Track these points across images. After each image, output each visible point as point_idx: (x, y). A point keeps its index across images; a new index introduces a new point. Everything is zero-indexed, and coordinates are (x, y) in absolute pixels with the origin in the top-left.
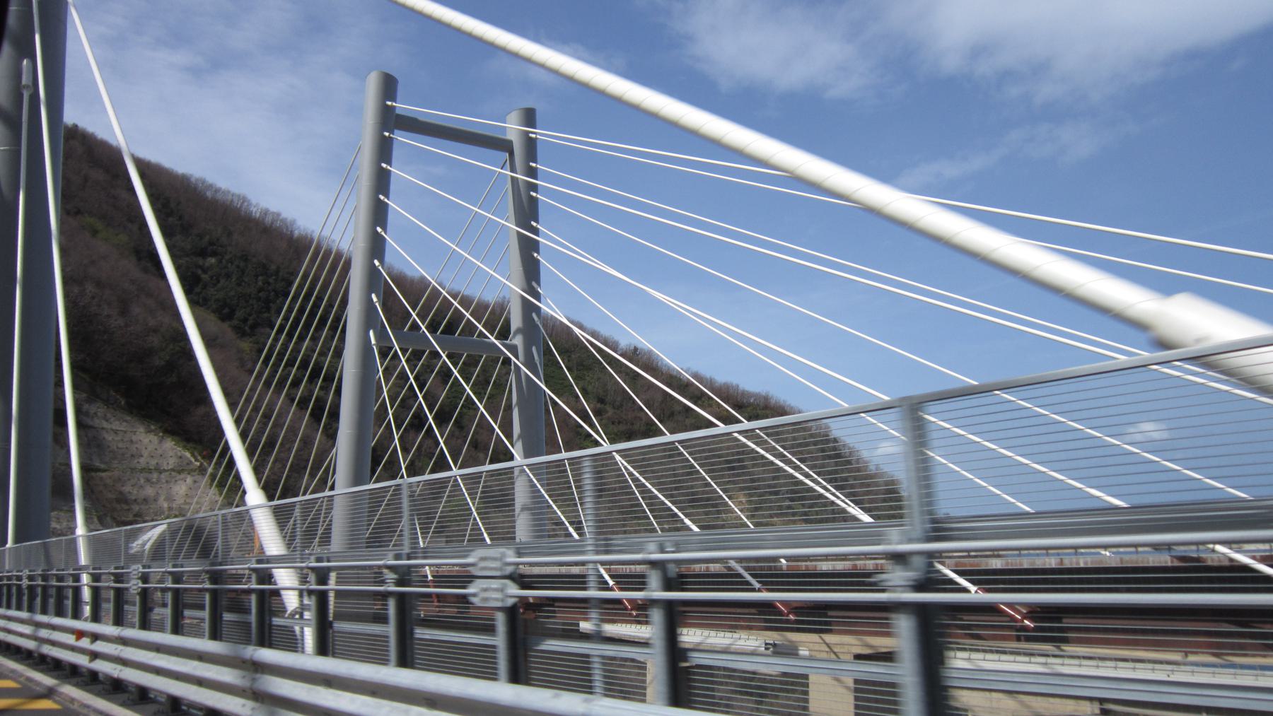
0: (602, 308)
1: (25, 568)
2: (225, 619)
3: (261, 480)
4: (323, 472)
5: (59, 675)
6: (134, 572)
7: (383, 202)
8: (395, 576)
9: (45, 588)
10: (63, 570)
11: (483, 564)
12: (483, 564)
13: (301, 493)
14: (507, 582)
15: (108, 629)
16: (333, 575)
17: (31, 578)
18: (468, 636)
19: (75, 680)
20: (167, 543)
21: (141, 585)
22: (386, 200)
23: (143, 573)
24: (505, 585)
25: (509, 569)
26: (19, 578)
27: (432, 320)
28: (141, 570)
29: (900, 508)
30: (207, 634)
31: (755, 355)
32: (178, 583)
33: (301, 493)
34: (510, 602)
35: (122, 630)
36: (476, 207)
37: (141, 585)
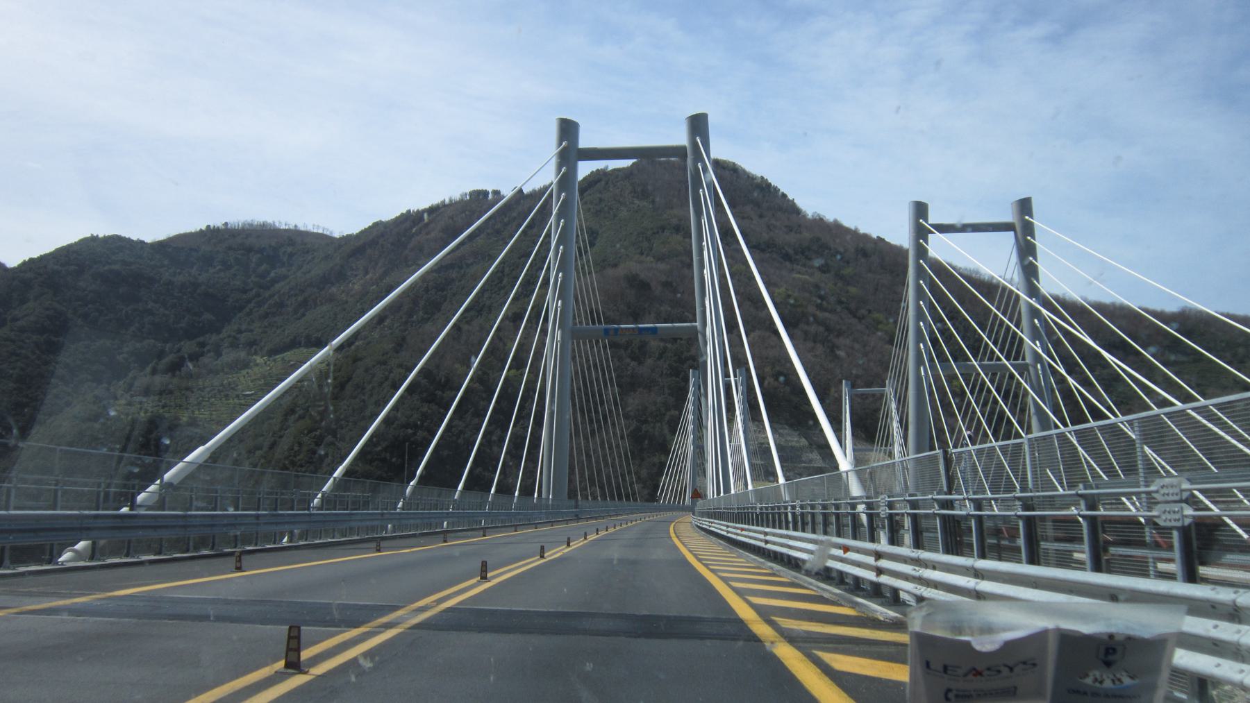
0: (1184, 298)
1: (797, 499)
2: (1042, 547)
3: (1007, 421)
4: (1110, 405)
5: (883, 603)
6: (882, 501)
7: (1028, 221)
8: (1021, 503)
9: (802, 514)
10: (827, 501)
11: (1162, 491)
12: (1162, 491)
13: (1001, 438)
14: (1184, 505)
15: (905, 551)
16: (789, 507)
17: (802, 507)
18: (1129, 550)
19: (880, 600)
20: (1139, 462)
21: (888, 511)
22: (1030, 219)
23: (889, 502)
24: (1182, 508)
25: (1185, 495)
26: (813, 507)
27: (1016, 322)
28: (887, 499)
29: (612, 498)
30: (1024, 562)
31: (1205, 350)
32: (915, 509)
33: (1001, 438)
34: (1187, 521)
35: (921, 553)
36: (730, 381)
37: (888, 511)
